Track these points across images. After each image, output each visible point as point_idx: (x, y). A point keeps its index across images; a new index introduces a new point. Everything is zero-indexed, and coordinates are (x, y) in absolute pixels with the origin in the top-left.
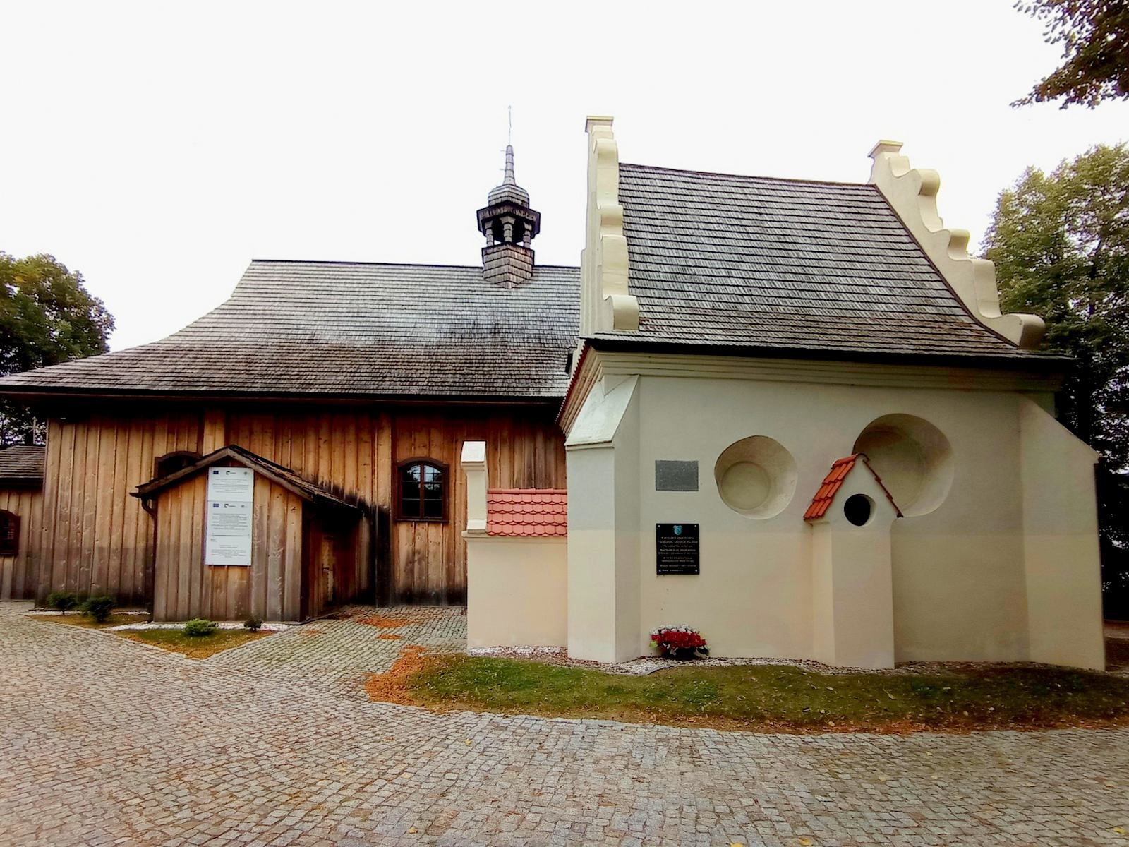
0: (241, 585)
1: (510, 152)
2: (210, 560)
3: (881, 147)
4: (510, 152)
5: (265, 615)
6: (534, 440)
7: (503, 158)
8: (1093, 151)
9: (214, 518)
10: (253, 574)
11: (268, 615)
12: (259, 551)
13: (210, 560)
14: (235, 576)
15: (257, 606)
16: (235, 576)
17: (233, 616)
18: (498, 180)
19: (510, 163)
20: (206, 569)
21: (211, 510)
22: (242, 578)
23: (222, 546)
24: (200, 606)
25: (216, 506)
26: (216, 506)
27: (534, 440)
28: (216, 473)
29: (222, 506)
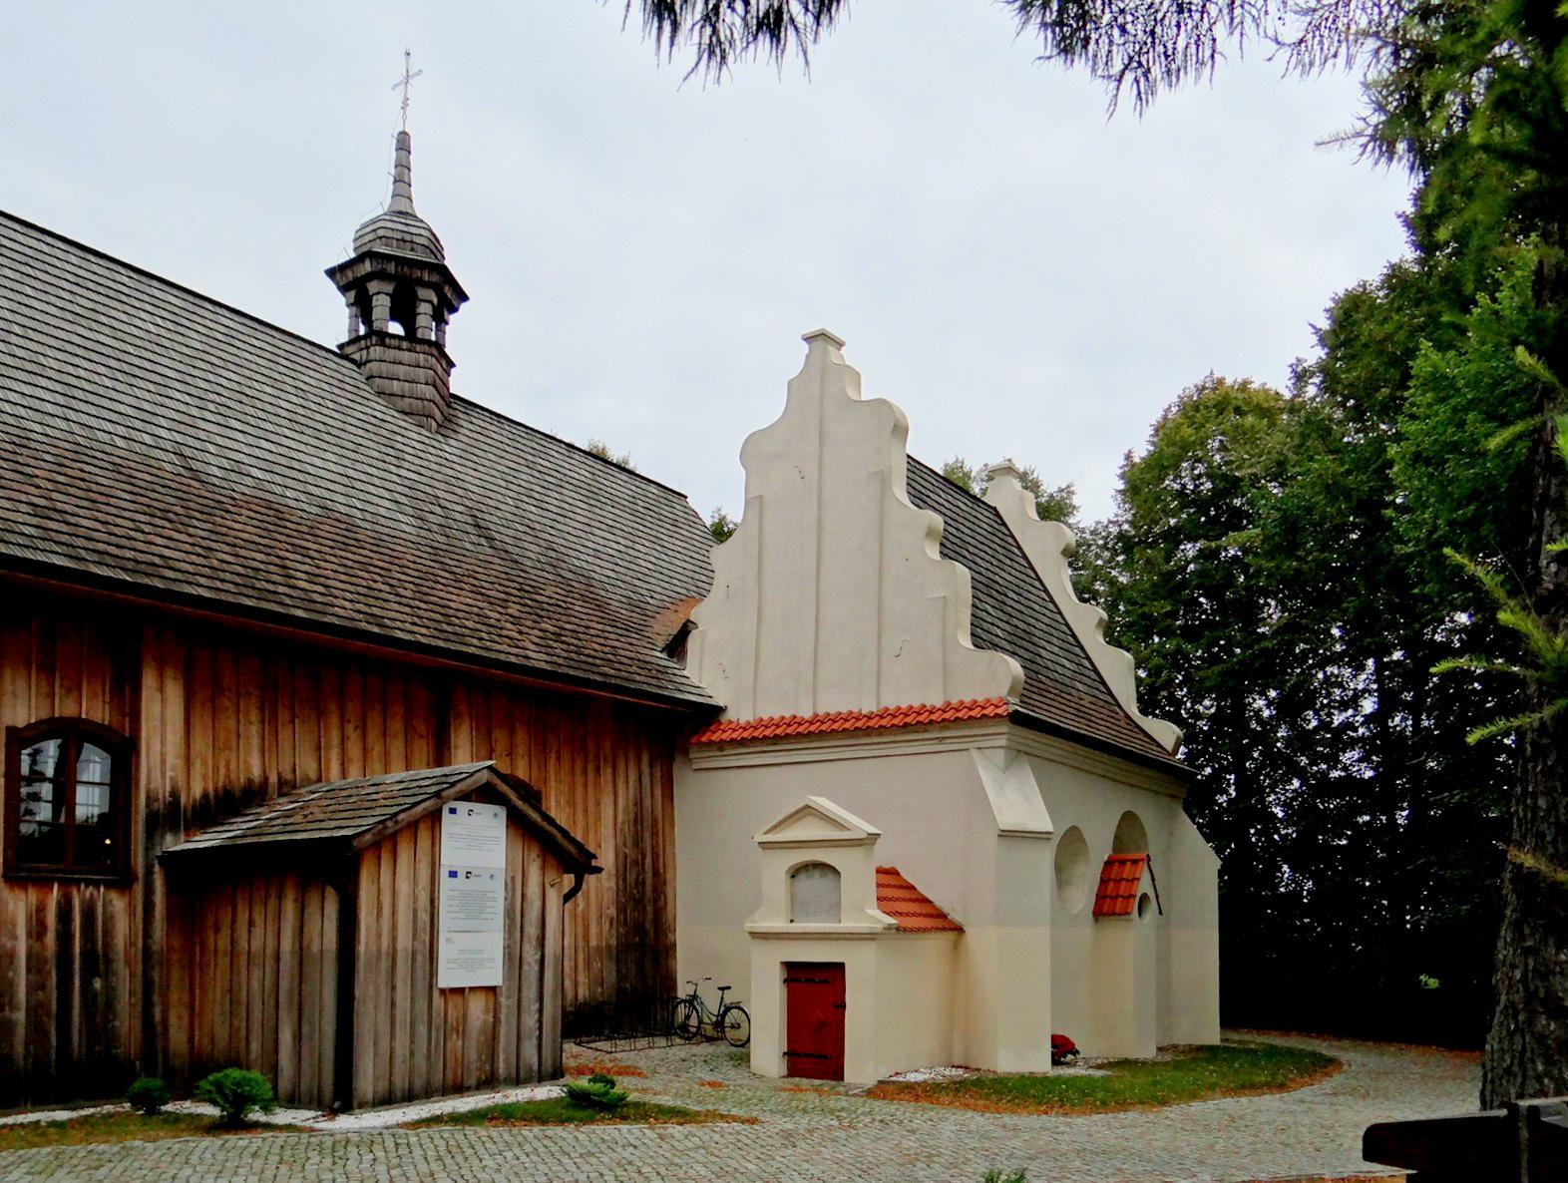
0: (485, 1022)
1: (403, 144)
2: (446, 979)
3: (815, 338)
4: (403, 144)
5: (518, 1073)
6: (26, 890)
7: (392, 156)
8: (1121, 486)
9: (451, 898)
10: (503, 1000)
11: (522, 1075)
12: (514, 961)
13: (446, 979)
14: (477, 1007)
15: (508, 1067)
16: (477, 1007)
17: (473, 1082)
18: (376, 201)
19: (403, 166)
20: (436, 994)
21: (445, 883)
22: (487, 1011)
23: (462, 951)
24: (428, 1071)
25: (453, 874)
26: (453, 874)
27: (26, 890)
28: (453, 811)
29: (461, 875)
